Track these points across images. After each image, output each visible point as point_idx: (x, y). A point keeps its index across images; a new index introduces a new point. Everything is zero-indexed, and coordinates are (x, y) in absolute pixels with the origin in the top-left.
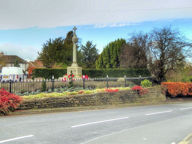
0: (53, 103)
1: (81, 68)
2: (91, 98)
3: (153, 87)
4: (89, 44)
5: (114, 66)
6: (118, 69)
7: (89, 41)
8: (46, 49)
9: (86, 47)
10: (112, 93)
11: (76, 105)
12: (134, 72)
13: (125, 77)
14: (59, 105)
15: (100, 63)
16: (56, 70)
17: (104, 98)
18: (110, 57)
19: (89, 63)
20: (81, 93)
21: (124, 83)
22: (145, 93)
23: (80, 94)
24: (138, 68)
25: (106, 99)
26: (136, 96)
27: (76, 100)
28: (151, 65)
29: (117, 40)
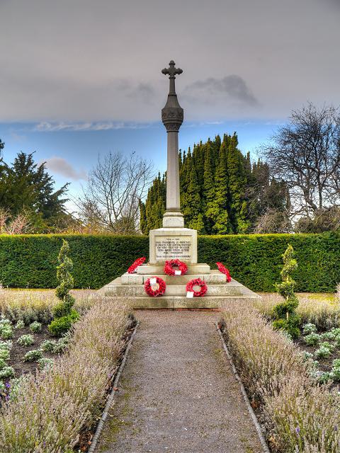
5: (218, 226)
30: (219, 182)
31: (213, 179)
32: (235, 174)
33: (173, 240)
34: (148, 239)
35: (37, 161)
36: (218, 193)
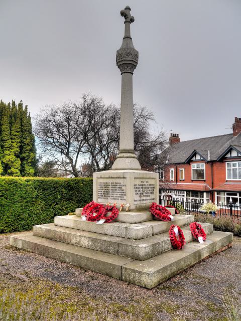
34: (92, 180)
36: (14, 144)
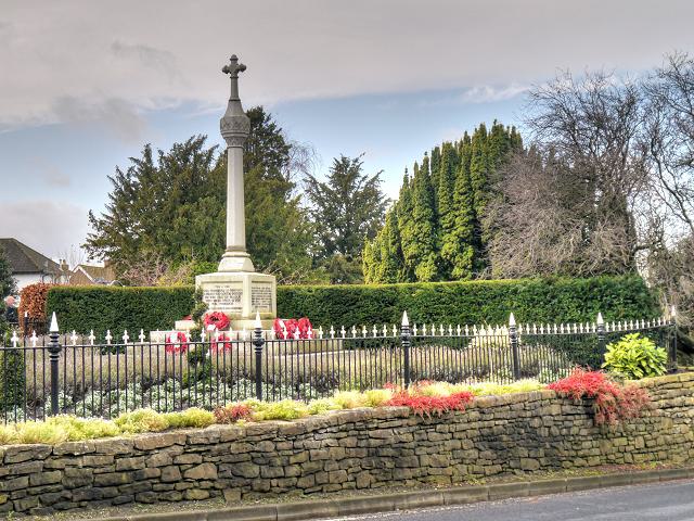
0: (37, 480)
1: (270, 283)
2: (297, 444)
3: (674, 377)
4: (345, 173)
5: (457, 271)
6: (479, 281)
7: (344, 159)
8: (126, 197)
9: (330, 187)
10: (432, 418)
11: (197, 493)
12: (565, 298)
13: (512, 321)
14: (83, 495)
15: (384, 254)
16: (150, 294)
17: (382, 447)
18: (435, 219)
19: (346, 266)
20: (234, 420)
21: (508, 359)
22: (631, 410)
23: (229, 427)
24: (586, 275)
25: (390, 452)
26: (574, 430)
27: (198, 458)
28: (661, 257)
29: (471, 134)
30: (459, 202)
31: (451, 198)
32: (480, 188)
33: (223, 287)
35: (367, 171)
